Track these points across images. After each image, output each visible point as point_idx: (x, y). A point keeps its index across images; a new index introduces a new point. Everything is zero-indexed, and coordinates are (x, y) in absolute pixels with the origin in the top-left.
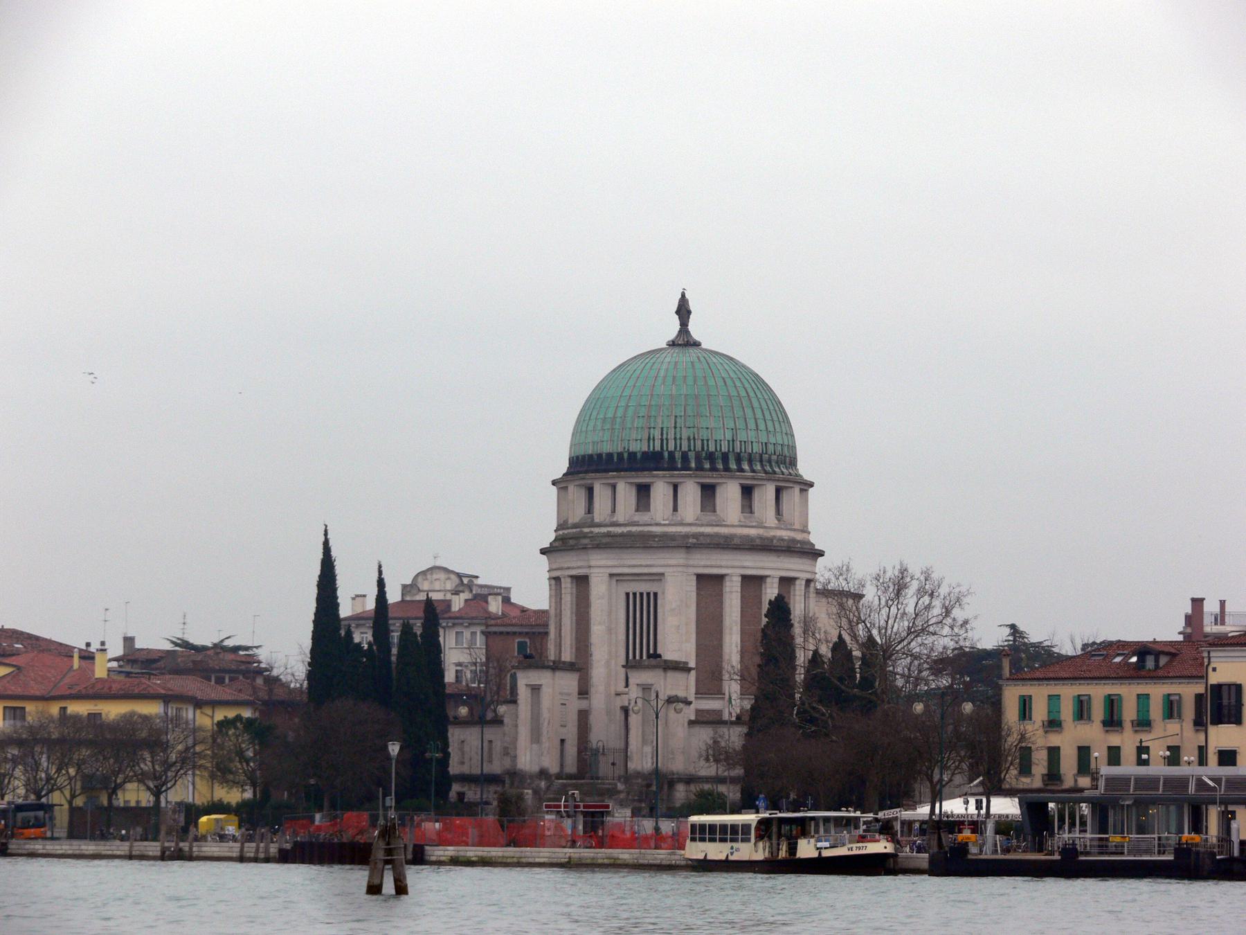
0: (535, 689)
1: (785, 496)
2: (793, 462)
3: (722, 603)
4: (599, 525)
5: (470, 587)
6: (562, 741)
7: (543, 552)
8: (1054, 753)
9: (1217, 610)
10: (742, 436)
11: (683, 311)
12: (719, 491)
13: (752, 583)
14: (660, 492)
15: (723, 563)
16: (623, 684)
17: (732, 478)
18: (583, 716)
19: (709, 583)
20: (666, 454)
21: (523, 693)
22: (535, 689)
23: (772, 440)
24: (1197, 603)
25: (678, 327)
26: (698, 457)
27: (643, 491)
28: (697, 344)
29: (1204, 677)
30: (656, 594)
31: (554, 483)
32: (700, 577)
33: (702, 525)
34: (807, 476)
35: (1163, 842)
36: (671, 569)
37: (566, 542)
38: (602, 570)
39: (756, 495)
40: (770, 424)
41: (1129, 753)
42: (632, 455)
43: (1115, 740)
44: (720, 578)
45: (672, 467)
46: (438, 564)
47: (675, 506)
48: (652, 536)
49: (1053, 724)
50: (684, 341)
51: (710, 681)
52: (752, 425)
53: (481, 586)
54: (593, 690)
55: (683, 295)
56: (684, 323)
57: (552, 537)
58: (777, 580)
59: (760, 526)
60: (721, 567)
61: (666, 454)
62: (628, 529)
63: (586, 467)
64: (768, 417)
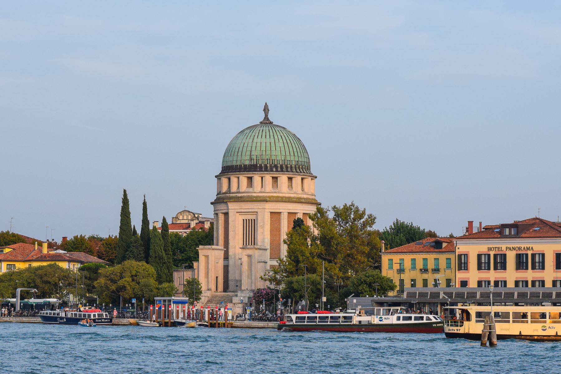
0: (207, 257)
1: (305, 181)
2: (308, 168)
4: (233, 193)
5: (198, 218)
6: (217, 277)
7: (212, 203)
8: (402, 281)
9: (479, 226)
10: (288, 158)
11: (266, 109)
12: (279, 178)
14: (257, 178)
15: (281, 208)
18: (226, 268)
19: (275, 215)
21: (202, 258)
22: (207, 257)
24: (470, 223)
26: (287, 167)
27: (250, 179)
28: (271, 123)
29: (454, 252)
32: (469, 222)
34: (314, 174)
37: (221, 200)
39: (294, 180)
41: (431, 283)
42: (245, 166)
43: (425, 276)
45: (261, 170)
47: (262, 184)
49: (401, 271)
50: (266, 122)
52: (292, 154)
53: (202, 218)
54: (229, 258)
55: (266, 104)
56: (266, 116)
59: (295, 193)
63: (228, 170)
64: (298, 151)
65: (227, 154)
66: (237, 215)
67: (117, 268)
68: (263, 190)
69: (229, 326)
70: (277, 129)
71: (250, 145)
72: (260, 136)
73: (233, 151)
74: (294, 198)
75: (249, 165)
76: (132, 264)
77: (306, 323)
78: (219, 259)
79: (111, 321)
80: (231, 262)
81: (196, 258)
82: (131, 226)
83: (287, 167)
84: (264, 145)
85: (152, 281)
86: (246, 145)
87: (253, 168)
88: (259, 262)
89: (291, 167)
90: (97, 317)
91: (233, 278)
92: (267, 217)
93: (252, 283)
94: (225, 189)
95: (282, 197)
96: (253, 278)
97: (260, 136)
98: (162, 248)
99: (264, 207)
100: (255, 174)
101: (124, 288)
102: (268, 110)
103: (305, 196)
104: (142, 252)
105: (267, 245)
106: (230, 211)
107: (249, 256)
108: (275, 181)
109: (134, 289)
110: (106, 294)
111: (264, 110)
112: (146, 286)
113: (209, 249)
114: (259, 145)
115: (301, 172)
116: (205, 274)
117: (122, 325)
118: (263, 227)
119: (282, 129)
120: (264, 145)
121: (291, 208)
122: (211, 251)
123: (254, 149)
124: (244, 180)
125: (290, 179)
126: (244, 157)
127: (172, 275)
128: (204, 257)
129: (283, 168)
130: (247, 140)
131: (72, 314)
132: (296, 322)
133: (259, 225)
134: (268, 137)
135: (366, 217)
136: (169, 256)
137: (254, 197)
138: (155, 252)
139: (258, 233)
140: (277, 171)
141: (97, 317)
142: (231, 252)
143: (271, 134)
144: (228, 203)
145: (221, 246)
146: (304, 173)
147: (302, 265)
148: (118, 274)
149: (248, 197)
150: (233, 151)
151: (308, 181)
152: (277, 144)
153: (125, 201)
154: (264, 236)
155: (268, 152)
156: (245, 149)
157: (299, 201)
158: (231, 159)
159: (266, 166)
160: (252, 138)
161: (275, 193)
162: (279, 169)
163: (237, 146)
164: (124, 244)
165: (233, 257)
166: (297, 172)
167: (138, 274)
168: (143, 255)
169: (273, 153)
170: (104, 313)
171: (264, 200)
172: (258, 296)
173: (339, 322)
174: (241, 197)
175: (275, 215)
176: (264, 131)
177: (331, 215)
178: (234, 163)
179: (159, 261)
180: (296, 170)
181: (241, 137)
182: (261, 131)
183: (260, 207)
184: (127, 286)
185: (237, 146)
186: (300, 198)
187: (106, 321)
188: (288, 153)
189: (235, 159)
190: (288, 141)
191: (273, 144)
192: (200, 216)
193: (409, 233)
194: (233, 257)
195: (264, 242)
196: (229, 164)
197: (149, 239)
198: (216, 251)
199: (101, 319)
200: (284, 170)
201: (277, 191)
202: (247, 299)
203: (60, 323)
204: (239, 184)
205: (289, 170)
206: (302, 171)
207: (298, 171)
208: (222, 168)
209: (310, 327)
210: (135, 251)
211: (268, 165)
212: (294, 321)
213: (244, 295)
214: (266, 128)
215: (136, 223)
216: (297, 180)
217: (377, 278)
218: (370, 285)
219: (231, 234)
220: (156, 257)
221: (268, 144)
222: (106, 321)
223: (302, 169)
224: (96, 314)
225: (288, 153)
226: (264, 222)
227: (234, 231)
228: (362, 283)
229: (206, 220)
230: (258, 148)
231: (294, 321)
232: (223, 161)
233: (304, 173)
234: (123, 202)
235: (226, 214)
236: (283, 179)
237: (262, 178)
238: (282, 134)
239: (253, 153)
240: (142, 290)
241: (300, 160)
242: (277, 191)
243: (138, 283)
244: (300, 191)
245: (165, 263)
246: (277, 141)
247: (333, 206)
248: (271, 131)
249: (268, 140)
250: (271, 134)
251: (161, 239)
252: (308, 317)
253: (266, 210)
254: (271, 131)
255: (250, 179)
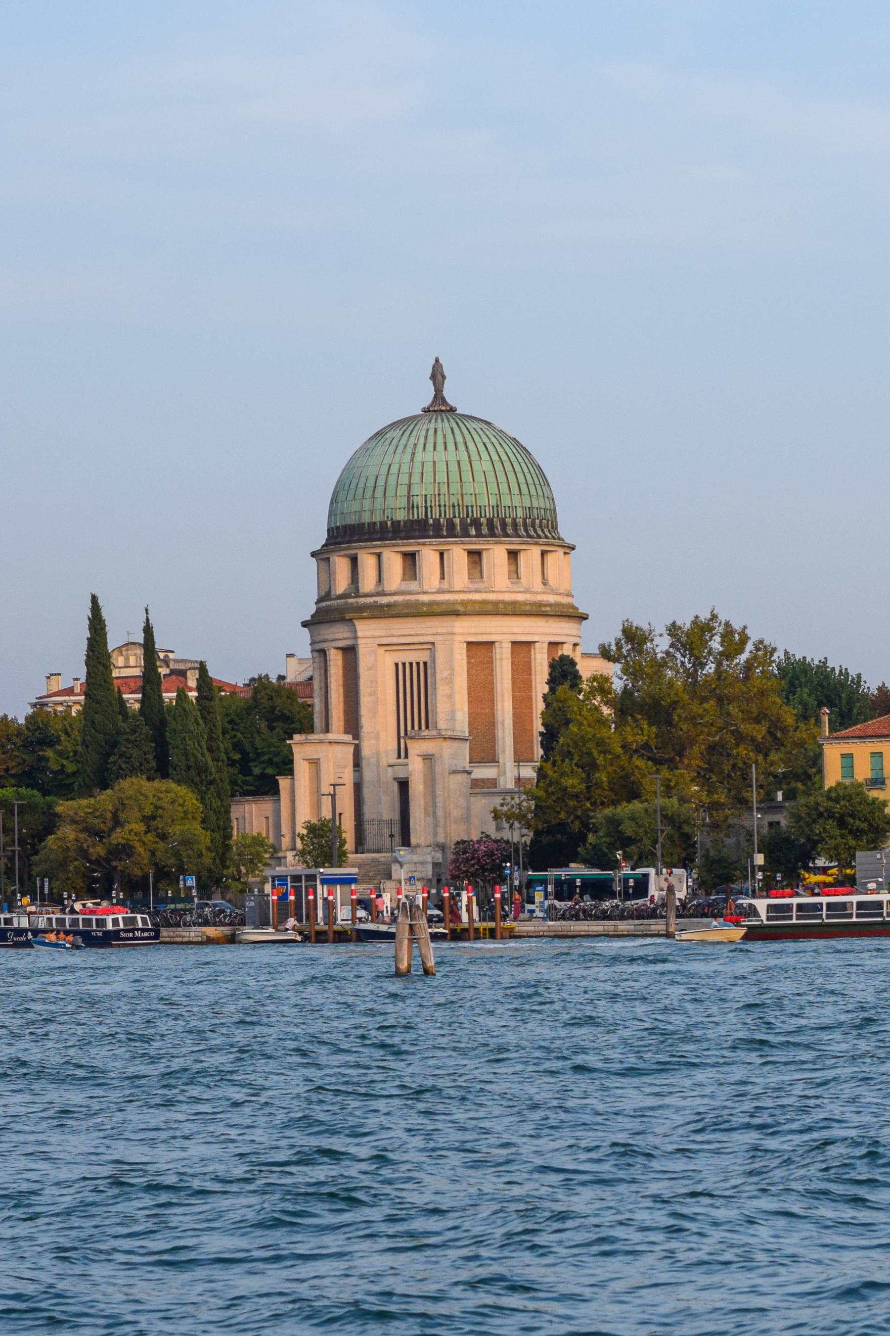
0: (315, 763)
1: (550, 559)
2: (554, 527)
3: (492, 670)
7: (305, 624)
10: (506, 501)
11: (437, 376)
12: (485, 555)
13: (522, 648)
14: (428, 556)
16: (396, 755)
17: (497, 543)
19: (481, 650)
20: (431, 521)
21: (301, 767)
22: (315, 763)
23: (535, 504)
25: (432, 393)
26: (504, 525)
27: (410, 559)
28: (452, 410)
30: (425, 663)
31: (313, 555)
33: (470, 592)
34: (569, 540)
35: (283, 860)
36: (439, 638)
37: (330, 613)
38: (369, 641)
39: (522, 557)
40: (532, 487)
42: (396, 524)
44: (530, 644)
46: (131, 640)
47: (443, 571)
48: (418, 604)
50: (440, 407)
51: (483, 749)
52: (515, 490)
53: (177, 661)
55: (437, 360)
56: (439, 391)
57: (313, 609)
58: (546, 645)
60: (423, 635)
61: (431, 521)
62: (375, 599)
63: (346, 536)
65: (342, 496)
66: (380, 654)
67: (105, 799)
68: (445, 586)
69: (506, 934)
70: (472, 425)
71: (405, 469)
72: (430, 446)
73: (361, 485)
74: (525, 603)
75: (405, 522)
76: (137, 788)
77: (794, 921)
78: (345, 767)
79: (157, 937)
80: (368, 774)
81: (287, 767)
82: (113, 691)
83: (504, 525)
84: (441, 467)
85: (196, 828)
86: (394, 470)
87: (413, 530)
88: (455, 772)
89: (515, 525)
90: (122, 926)
91: (374, 816)
92: (460, 655)
93: (436, 826)
94: (342, 584)
95: (496, 603)
96: (440, 813)
97: (430, 446)
98: (203, 743)
99: (449, 630)
100: (423, 544)
101: (126, 850)
102: (444, 377)
103: (552, 599)
104: (150, 757)
105: (462, 726)
106: (360, 641)
107: (428, 758)
108: (474, 562)
109: (153, 853)
110: (76, 867)
111: (433, 377)
112: (187, 842)
113: (321, 742)
114: (429, 468)
115: (539, 537)
116: (312, 807)
117: (182, 943)
118: (450, 681)
119: (484, 426)
120: (441, 467)
121: (519, 630)
122: (325, 747)
123: (416, 479)
124: (394, 562)
125: (513, 555)
126: (390, 502)
127: (228, 812)
128: (306, 765)
129: (495, 527)
130: (397, 458)
131: (50, 920)
132: (768, 919)
133: (438, 677)
134: (451, 446)
135: (749, 647)
136: (220, 764)
137: (424, 604)
138: (186, 754)
139: (439, 697)
140: (479, 535)
141: (122, 926)
142: (366, 752)
143: (459, 439)
144: (356, 622)
145: (337, 733)
146: (547, 537)
147: (602, 777)
148: (109, 815)
149: (408, 604)
150: (361, 485)
151: (556, 558)
152: (476, 465)
153: (97, 624)
154: (453, 705)
155: (455, 488)
156: (392, 480)
157: (537, 611)
158: (356, 506)
159: (451, 525)
160: (409, 450)
161: (477, 591)
162: (485, 530)
163: (371, 472)
164: (100, 737)
165: (373, 761)
166: (529, 536)
167: (160, 812)
168: (153, 764)
169: (469, 489)
170: (139, 916)
171: (452, 612)
172: (467, 860)
173: (881, 915)
174: (389, 605)
175: (481, 650)
176: (439, 432)
177: (662, 644)
178: (366, 518)
179: (197, 779)
180: (526, 530)
181: (380, 450)
182: (431, 432)
183: (440, 630)
184: (137, 844)
185: (371, 472)
186: (540, 604)
187: (146, 934)
188: (504, 488)
189: (367, 505)
190: (504, 458)
191: (465, 466)
192: (171, 656)
193: (823, 687)
194: (373, 761)
195: (453, 719)
196: (352, 520)
197: (163, 723)
198: (338, 748)
199: (132, 931)
200: (498, 530)
201: (480, 586)
202: (429, 868)
203: (17, 945)
204: (381, 570)
205: (510, 531)
206: (540, 533)
207: (532, 533)
208: (328, 530)
209: (778, 931)
210: (135, 753)
211: (457, 521)
212: (763, 916)
213: (421, 859)
214: (444, 425)
215: (127, 666)
216: (531, 556)
217: (860, 803)
218: (841, 823)
219: (365, 701)
220: (189, 768)
221: (454, 467)
222: (146, 934)
223: (536, 528)
224: (120, 917)
225: (504, 488)
226: (453, 669)
227: (373, 694)
228: (821, 815)
229: (189, 665)
230: (428, 478)
231: (763, 916)
232: (332, 514)
233: (547, 537)
234: (90, 629)
235: (350, 652)
236: (496, 555)
237: (442, 555)
238: (486, 440)
239: (415, 490)
240: (177, 854)
241: (535, 504)
242: (480, 586)
243: (163, 837)
244: (538, 585)
245: (211, 783)
246: (475, 457)
247: (669, 622)
248: (457, 431)
249: (452, 456)
250: (459, 439)
251: (201, 721)
252: (828, 904)
253: (456, 638)
254: (457, 431)
255: (410, 559)
